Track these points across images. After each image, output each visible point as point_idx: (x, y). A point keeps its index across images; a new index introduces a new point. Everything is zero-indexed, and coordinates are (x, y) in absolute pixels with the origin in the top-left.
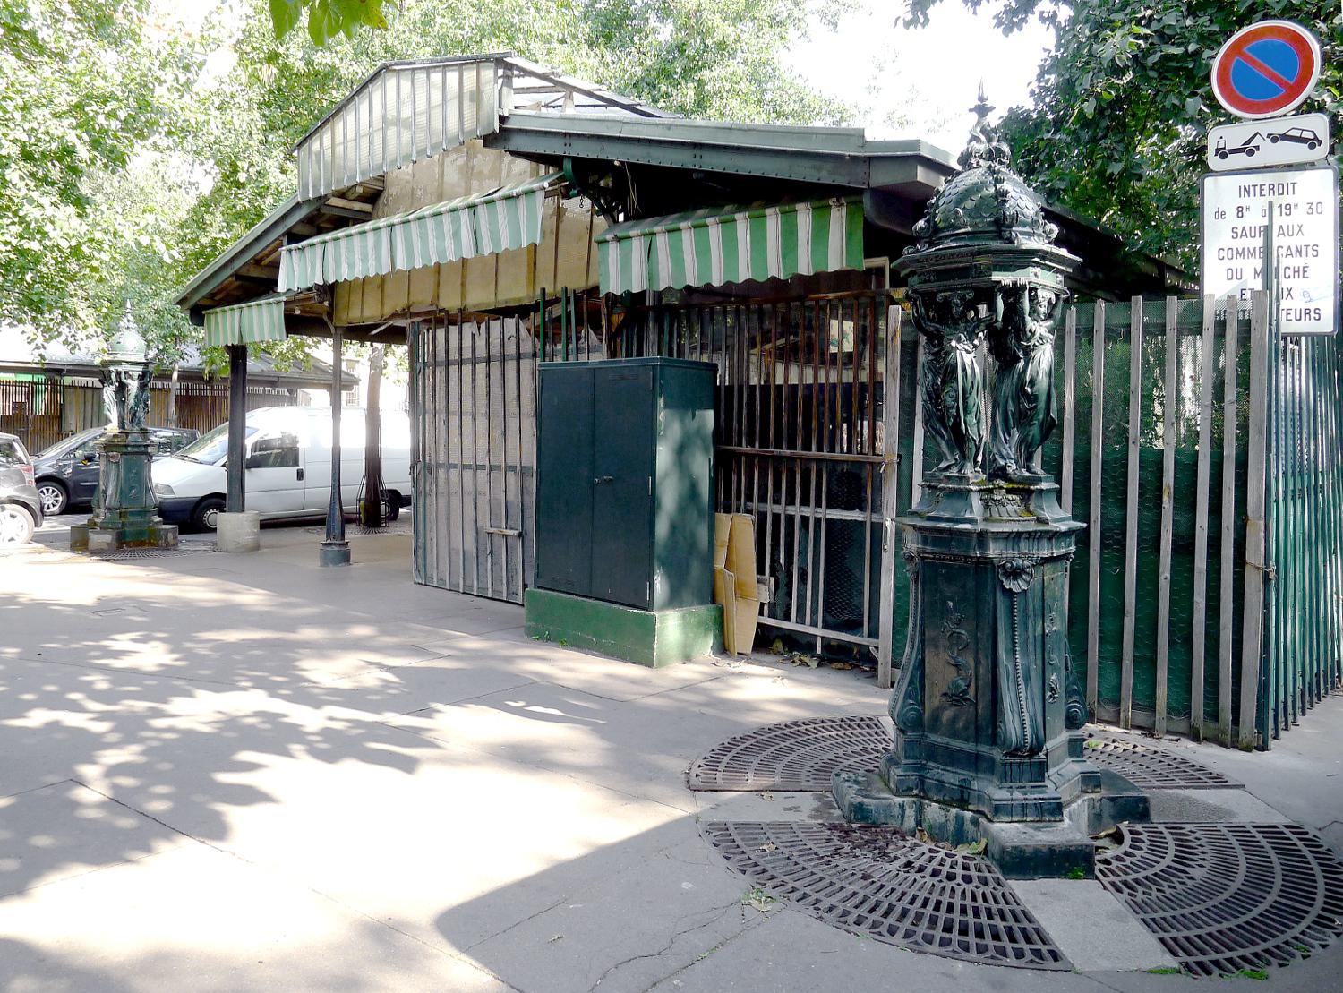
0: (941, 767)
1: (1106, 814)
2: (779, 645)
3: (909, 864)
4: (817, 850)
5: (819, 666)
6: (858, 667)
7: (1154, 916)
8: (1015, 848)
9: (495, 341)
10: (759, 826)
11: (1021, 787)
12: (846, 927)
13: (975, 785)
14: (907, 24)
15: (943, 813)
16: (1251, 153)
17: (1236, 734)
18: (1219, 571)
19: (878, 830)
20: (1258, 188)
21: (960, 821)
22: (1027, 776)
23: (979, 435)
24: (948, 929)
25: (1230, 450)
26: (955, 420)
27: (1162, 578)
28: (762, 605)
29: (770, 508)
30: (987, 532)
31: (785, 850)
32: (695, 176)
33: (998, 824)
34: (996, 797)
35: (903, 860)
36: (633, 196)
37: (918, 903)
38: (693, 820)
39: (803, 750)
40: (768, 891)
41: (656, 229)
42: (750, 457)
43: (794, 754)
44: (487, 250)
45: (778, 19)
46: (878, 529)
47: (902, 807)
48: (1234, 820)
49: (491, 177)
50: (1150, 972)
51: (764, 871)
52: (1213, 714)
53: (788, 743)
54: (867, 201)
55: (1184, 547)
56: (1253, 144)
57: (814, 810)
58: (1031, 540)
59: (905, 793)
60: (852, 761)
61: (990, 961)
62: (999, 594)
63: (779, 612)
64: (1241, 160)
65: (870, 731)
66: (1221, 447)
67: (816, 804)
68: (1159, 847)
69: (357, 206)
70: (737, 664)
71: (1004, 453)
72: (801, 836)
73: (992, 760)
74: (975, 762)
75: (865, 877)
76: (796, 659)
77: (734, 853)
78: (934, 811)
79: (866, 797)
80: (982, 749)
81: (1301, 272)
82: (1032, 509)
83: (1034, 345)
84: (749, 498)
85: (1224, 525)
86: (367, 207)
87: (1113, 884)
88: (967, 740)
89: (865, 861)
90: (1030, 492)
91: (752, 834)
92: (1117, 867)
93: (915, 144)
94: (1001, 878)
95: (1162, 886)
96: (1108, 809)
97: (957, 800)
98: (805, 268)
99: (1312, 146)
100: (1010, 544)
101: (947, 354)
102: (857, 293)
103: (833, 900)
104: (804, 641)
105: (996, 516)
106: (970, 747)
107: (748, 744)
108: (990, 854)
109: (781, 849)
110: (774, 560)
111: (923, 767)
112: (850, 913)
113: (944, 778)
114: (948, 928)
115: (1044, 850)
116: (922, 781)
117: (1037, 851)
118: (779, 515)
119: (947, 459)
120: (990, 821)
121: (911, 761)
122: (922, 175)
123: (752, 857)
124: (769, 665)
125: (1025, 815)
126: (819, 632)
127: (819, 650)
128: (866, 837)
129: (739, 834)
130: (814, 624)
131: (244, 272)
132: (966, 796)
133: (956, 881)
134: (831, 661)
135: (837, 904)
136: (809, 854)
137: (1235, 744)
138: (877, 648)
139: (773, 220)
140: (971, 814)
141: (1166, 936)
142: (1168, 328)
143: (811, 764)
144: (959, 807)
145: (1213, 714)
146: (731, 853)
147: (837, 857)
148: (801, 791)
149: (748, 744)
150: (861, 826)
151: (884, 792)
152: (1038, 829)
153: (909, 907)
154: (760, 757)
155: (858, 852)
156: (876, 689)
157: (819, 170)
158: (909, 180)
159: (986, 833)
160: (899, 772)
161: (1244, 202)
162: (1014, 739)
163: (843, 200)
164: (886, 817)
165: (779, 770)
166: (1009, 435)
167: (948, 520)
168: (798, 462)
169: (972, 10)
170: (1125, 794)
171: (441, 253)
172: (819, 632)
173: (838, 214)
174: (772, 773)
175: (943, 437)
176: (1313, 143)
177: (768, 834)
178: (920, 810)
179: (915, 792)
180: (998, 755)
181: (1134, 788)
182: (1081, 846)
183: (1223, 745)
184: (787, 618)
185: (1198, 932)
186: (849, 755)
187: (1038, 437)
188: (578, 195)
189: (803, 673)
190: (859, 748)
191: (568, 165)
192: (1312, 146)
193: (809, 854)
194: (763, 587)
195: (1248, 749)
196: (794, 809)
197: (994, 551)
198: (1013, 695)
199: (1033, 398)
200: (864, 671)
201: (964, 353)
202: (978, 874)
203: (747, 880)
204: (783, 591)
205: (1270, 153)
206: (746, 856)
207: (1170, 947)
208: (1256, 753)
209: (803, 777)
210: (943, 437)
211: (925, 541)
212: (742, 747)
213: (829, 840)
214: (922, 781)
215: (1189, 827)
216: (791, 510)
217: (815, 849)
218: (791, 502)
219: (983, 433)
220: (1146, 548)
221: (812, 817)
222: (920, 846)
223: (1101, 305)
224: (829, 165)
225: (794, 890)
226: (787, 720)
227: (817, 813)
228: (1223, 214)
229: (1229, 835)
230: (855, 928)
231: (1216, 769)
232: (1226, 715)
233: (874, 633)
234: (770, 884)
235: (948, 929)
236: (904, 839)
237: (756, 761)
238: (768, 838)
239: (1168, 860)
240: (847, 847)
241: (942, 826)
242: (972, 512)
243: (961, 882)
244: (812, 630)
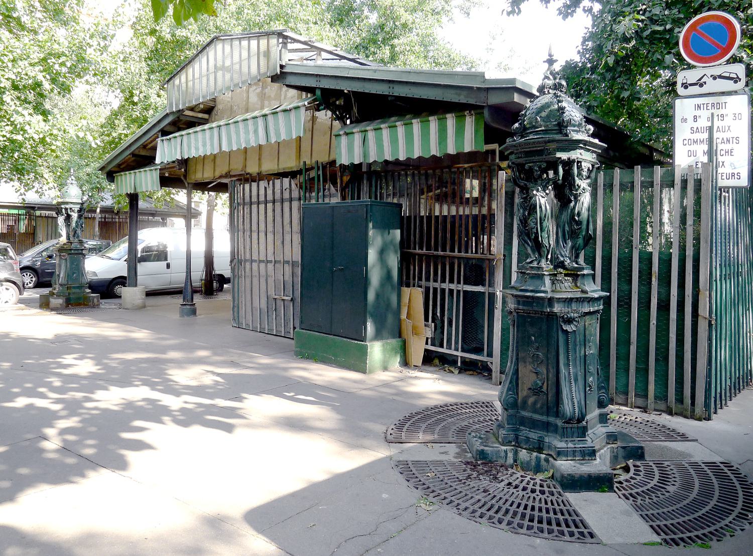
0: (528, 429)
1: (620, 456)
2: (437, 361)
3: (510, 484)
4: (458, 476)
5: (459, 373)
6: (481, 373)
7: (647, 513)
8: (569, 475)
9: (278, 191)
10: (426, 462)
11: (572, 441)
12: (474, 519)
13: (547, 440)
14: (509, 14)
15: (529, 455)
16: (701, 86)
17: (693, 411)
18: (683, 320)
19: (492, 465)
20: (705, 105)
21: (538, 460)
22: (576, 434)
23: (549, 243)
24: (531, 520)
25: (690, 252)
26: (535, 235)
27: (651, 324)
28: (427, 339)
29: (432, 284)
30: (553, 298)
31: (440, 476)
32: (389, 98)
33: (559, 462)
34: (558, 446)
35: (506, 482)
36: (355, 110)
37: (515, 505)
38: (389, 459)
39: (450, 420)
40: (431, 499)
41: (368, 128)
42: (421, 256)
43: (445, 422)
44: (273, 140)
45: (436, 11)
46: (492, 296)
47: (506, 452)
48: (692, 459)
49: (275, 99)
50: (645, 544)
51: (428, 488)
52: (680, 400)
53: (442, 416)
54: (486, 112)
55: (664, 307)
56: (703, 80)
57: (457, 453)
58: (578, 302)
59: (507, 444)
60: (478, 426)
61: (555, 538)
62: (560, 333)
63: (437, 343)
64: (696, 90)
65: (488, 409)
66: (685, 250)
67: (457, 450)
68: (650, 474)
69: (200, 115)
70: (413, 372)
71: (563, 253)
72: (449, 468)
73: (556, 426)
74: (547, 427)
75: (485, 491)
76: (446, 369)
77: (412, 478)
78: (523, 454)
79: (485, 446)
80: (551, 420)
81: (730, 152)
82: (578, 285)
83: (580, 193)
84: (420, 279)
85: (686, 294)
86: (206, 116)
87: (624, 495)
88: (542, 414)
89: (485, 482)
90: (578, 276)
91: (422, 467)
92: (626, 485)
93: (513, 81)
94: (561, 491)
95: (651, 496)
96: (621, 453)
97: (537, 448)
98: (451, 150)
99: (736, 82)
100: (566, 305)
101: (531, 198)
102: (481, 164)
103: (467, 504)
104: (451, 359)
105: (558, 289)
106: (544, 418)
107: (419, 416)
108: (555, 478)
109: (438, 476)
110: (434, 314)
111: (518, 430)
112: (476, 511)
113: (529, 436)
114: (531, 520)
115: (586, 476)
116: (517, 437)
117: (581, 477)
118: (437, 288)
119: (531, 257)
120: (555, 459)
121: (511, 426)
122: (517, 98)
123: (421, 480)
124: (431, 372)
125: (575, 456)
126: (459, 354)
127: (459, 364)
128: (486, 469)
129: (414, 467)
130: (457, 350)
131: (137, 152)
132: (541, 446)
133: (536, 494)
134: (466, 370)
135: (470, 506)
136: (453, 478)
137: (693, 416)
138: (492, 363)
139: (433, 123)
140: (544, 456)
141: (654, 524)
142: (655, 183)
143: (455, 428)
144: (537, 452)
145: (680, 400)
146: (410, 478)
147: (469, 480)
148: (449, 443)
149: (419, 416)
150: (483, 462)
151: (495, 443)
152: (582, 464)
153: (509, 508)
154: (426, 424)
155: (481, 477)
156: (491, 386)
157: (459, 95)
158: (510, 101)
159: (553, 467)
160: (504, 432)
161: (698, 113)
162: (568, 414)
163: (473, 112)
164: (497, 458)
165: (437, 431)
166: (566, 244)
167: (532, 291)
168: (448, 259)
169: (545, 6)
170: (631, 445)
171: (247, 141)
172: (459, 354)
173: (470, 120)
174: (433, 433)
175: (529, 245)
176: (736, 80)
177: (431, 467)
178: (516, 453)
179: (513, 443)
180: (559, 423)
181: (636, 441)
182: (606, 473)
183: (686, 417)
184: (442, 346)
185: (672, 522)
186: (476, 423)
187: (582, 245)
188: (324, 109)
189: (450, 377)
190: (482, 419)
191: (318, 93)
192: (736, 82)
193: (453, 478)
194: (428, 329)
195: (700, 419)
196: (445, 453)
197: (557, 308)
198: (568, 389)
199: (579, 223)
200: (485, 376)
201: (540, 198)
202: (548, 489)
203: (419, 493)
204: (439, 331)
205: (712, 86)
206: (418, 479)
207: (656, 530)
208: (704, 422)
209: (450, 435)
210: (529, 245)
211: (518, 303)
212: (416, 418)
213: (465, 471)
214: (517, 437)
215: (667, 463)
216: (444, 286)
217: (457, 475)
218: (443, 281)
219: (551, 242)
220: (643, 307)
221: (455, 457)
222: (516, 474)
223: (617, 171)
224: (465, 93)
225: (445, 498)
226: (441, 403)
227: (458, 455)
228: (686, 120)
229: (689, 468)
230: (479, 520)
231: (682, 430)
232: (687, 400)
233: (490, 355)
234: (432, 495)
235: (531, 520)
236: (507, 470)
237: (424, 426)
238: (431, 469)
239: (655, 482)
240: (475, 474)
241: (528, 463)
242: (545, 287)
243: (539, 494)
244: (455, 353)
